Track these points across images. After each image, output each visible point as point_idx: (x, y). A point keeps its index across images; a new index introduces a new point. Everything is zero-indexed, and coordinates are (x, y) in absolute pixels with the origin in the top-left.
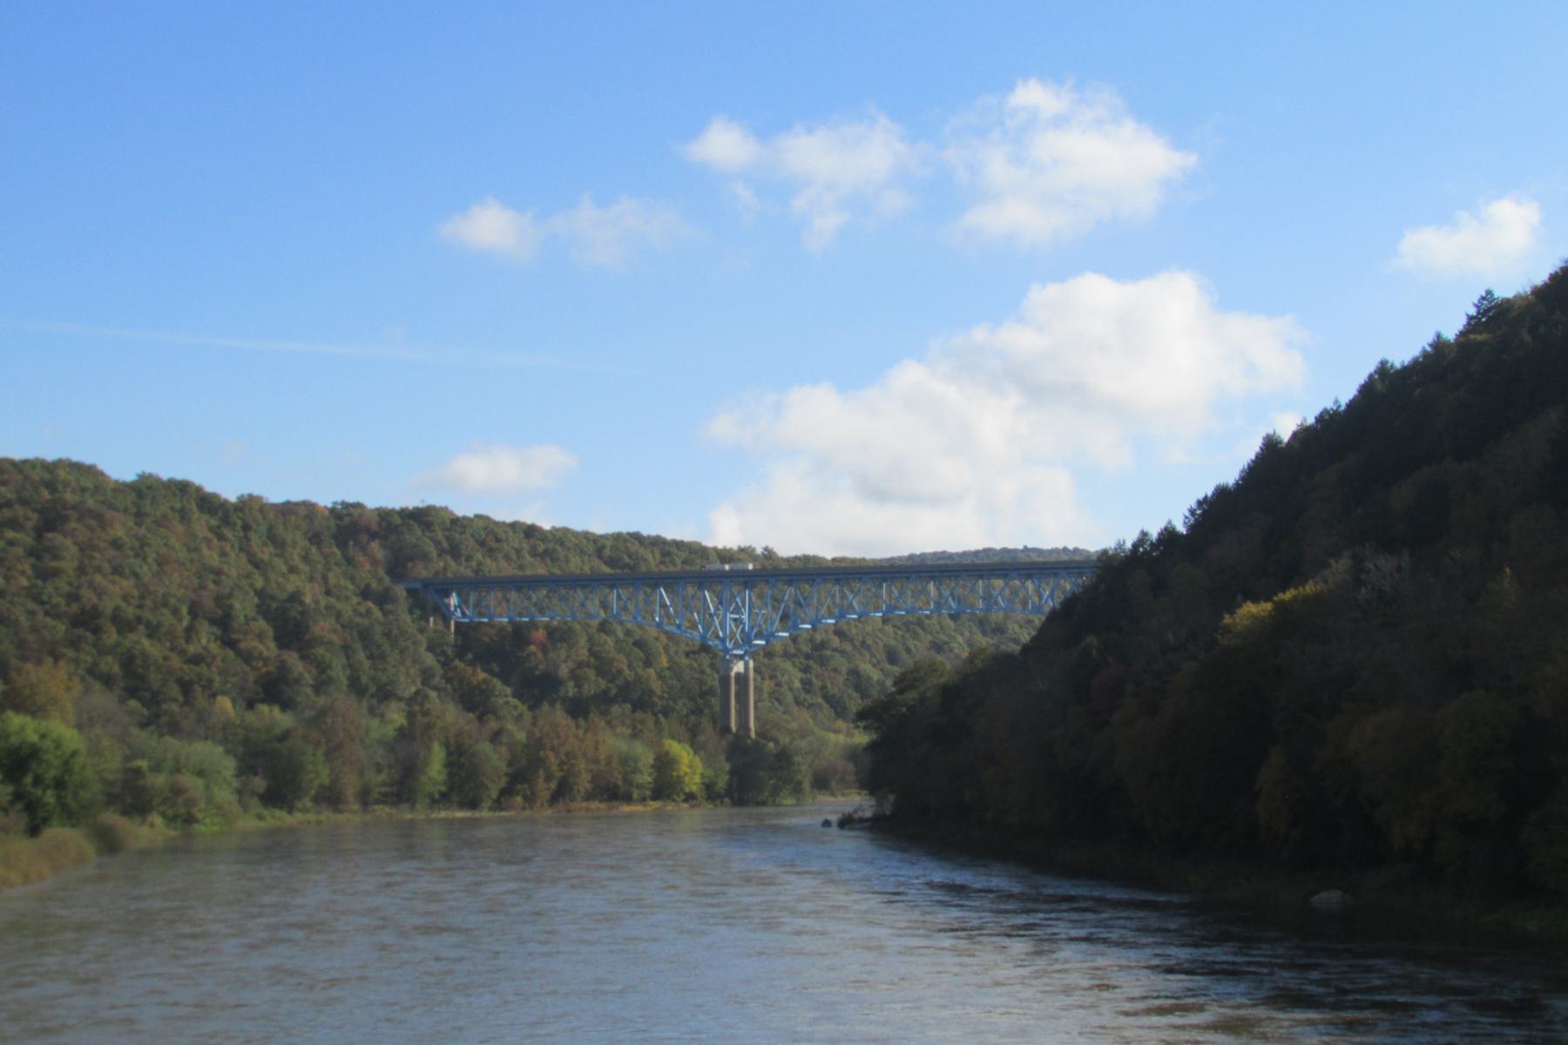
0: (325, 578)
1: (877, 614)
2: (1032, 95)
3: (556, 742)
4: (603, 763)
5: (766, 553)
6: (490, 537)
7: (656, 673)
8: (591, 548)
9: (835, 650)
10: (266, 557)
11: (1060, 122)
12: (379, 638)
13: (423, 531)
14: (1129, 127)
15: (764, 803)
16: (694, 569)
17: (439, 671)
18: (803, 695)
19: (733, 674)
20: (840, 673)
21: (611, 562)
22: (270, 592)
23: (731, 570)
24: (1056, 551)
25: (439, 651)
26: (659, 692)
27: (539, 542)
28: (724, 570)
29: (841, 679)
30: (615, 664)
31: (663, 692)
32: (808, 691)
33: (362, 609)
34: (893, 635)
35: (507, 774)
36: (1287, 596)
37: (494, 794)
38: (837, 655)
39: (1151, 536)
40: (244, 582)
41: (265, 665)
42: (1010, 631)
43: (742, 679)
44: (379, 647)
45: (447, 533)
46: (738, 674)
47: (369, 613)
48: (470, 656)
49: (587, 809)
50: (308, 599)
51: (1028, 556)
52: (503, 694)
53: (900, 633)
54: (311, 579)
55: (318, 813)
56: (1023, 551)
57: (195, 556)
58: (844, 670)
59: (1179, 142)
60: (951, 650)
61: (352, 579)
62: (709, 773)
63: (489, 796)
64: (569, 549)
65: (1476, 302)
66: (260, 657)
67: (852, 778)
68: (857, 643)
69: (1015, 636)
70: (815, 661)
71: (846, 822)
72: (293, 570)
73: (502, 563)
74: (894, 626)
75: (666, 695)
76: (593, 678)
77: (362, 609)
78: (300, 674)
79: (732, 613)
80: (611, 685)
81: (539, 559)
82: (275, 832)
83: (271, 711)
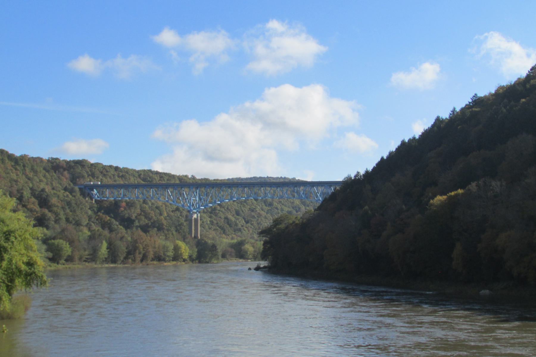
0: (52, 184)
1: (243, 199)
2: (274, 25)
3: (142, 241)
4: (157, 248)
5: (192, 177)
6: (104, 170)
7: (164, 218)
8: (137, 175)
9: (219, 210)
10: (31, 176)
11: (282, 34)
12: (74, 205)
13: (82, 168)
14: (304, 36)
15: (208, 263)
16: (171, 182)
17: (94, 216)
18: (211, 226)
19: (193, 218)
20: (222, 218)
21: (144, 180)
22: (35, 188)
23: (93, 184)
24: (277, 178)
25: (92, 209)
26: (165, 224)
27: (120, 172)
28: (91, 184)
29: (222, 220)
30: (151, 214)
31: (167, 224)
32: (212, 225)
33: (65, 195)
34: (237, 206)
35: (126, 252)
36: (453, 194)
37: (122, 258)
38: (221, 212)
39: (361, 173)
40: (26, 185)
41: (37, 213)
42: (274, 205)
43: (196, 220)
44: (74, 208)
45: (90, 169)
46: (195, 218)
47: (67, 196)
48: (103, 211)
49: (153, 264)
50: (47, 190)
51: (270, 180)
52: (115, 223)
53: (239, 205)
54: (47, 184)
55: (68, 264)
56: (266, 178)
57: (8, 175)
58: (223, 217)
59: (322, 42)
60: (256, 211)
61: (61, 184)
62: (191, 252)
63: (120, 259)
64: (130, 175)
65: (472, 98)
66: (35, 211)
67: (233, 254)
68: (226, 208)
69: (276, 207)
70: (213, 214)
71: (258, 269)
72: (41, 181)
73: (108, 179)
74: (237, 203)
75: (168, 225)
76: (143, 219)
77: (65, 195)
78: (50, 217)
79: (193, 198)
80: (149, 222)
81: (120, 178)
82: (55, 271)
83: (43, 229)
